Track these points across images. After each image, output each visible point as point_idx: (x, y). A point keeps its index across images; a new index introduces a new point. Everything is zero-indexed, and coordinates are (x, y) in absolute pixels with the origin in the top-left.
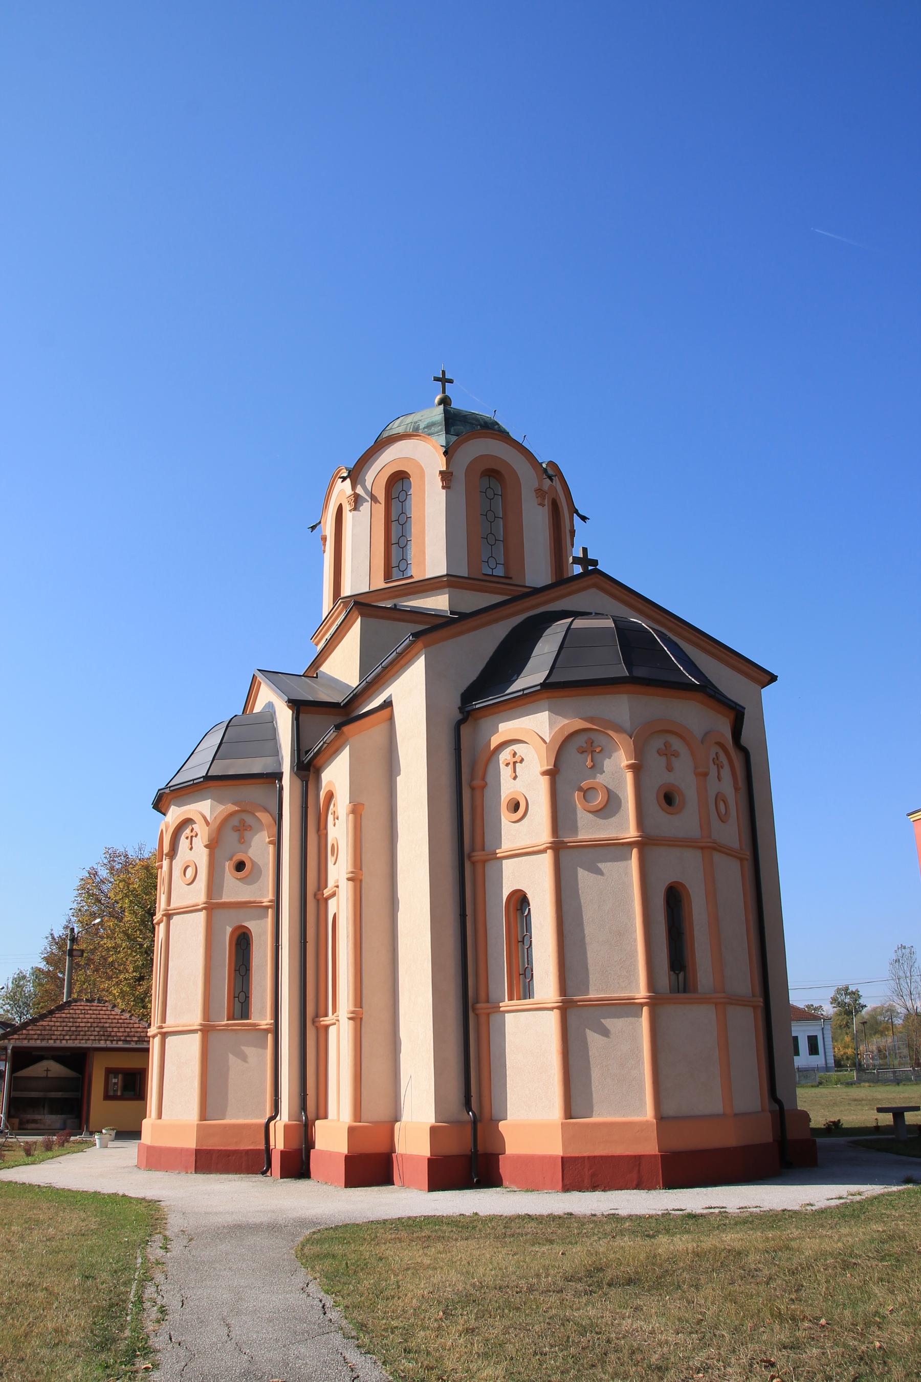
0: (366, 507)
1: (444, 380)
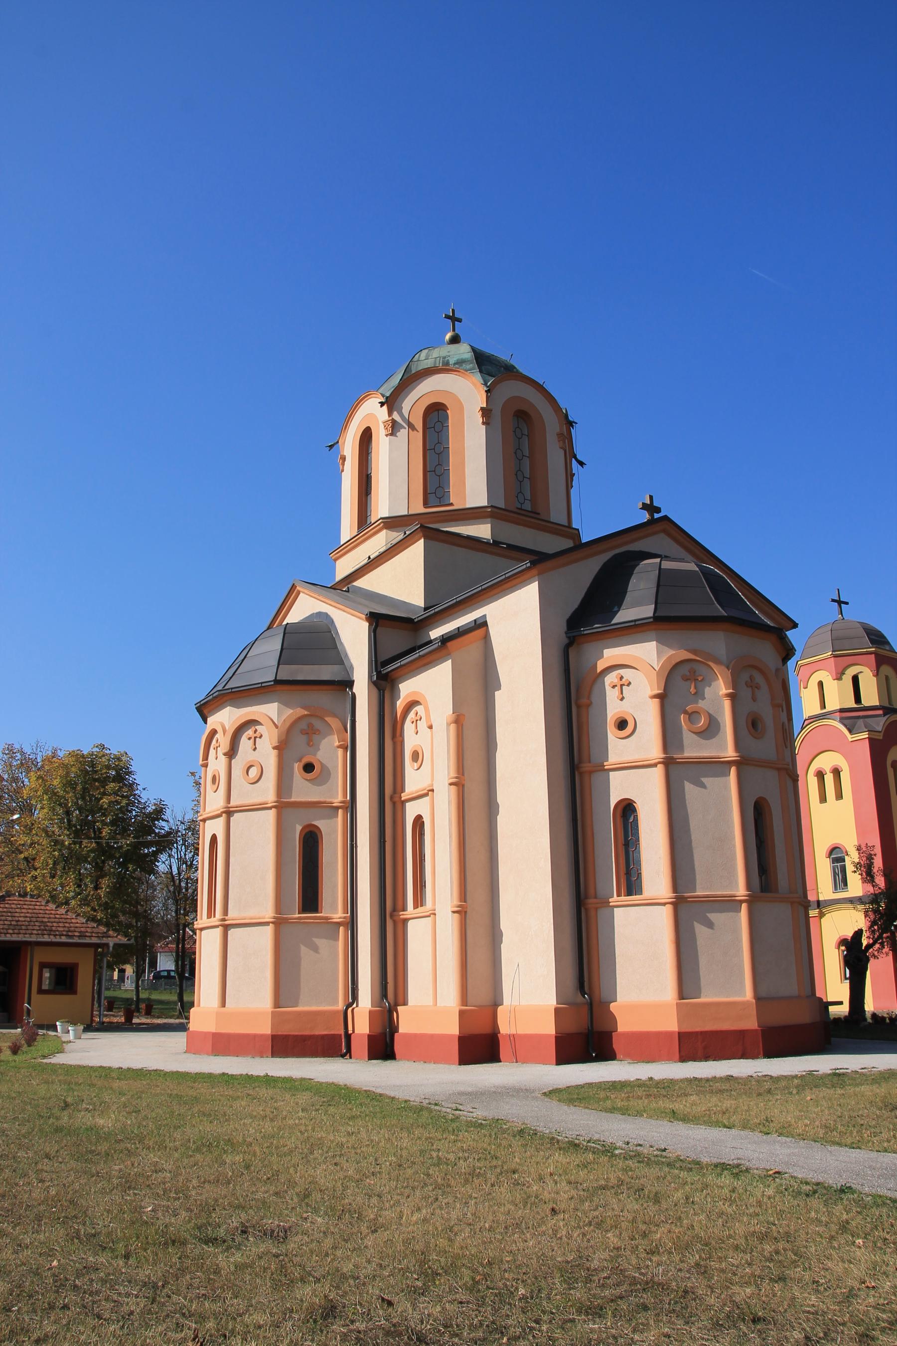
0: (403, 433)
1: (454, 319)
